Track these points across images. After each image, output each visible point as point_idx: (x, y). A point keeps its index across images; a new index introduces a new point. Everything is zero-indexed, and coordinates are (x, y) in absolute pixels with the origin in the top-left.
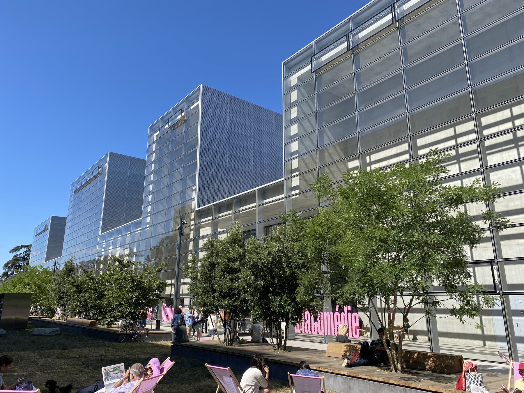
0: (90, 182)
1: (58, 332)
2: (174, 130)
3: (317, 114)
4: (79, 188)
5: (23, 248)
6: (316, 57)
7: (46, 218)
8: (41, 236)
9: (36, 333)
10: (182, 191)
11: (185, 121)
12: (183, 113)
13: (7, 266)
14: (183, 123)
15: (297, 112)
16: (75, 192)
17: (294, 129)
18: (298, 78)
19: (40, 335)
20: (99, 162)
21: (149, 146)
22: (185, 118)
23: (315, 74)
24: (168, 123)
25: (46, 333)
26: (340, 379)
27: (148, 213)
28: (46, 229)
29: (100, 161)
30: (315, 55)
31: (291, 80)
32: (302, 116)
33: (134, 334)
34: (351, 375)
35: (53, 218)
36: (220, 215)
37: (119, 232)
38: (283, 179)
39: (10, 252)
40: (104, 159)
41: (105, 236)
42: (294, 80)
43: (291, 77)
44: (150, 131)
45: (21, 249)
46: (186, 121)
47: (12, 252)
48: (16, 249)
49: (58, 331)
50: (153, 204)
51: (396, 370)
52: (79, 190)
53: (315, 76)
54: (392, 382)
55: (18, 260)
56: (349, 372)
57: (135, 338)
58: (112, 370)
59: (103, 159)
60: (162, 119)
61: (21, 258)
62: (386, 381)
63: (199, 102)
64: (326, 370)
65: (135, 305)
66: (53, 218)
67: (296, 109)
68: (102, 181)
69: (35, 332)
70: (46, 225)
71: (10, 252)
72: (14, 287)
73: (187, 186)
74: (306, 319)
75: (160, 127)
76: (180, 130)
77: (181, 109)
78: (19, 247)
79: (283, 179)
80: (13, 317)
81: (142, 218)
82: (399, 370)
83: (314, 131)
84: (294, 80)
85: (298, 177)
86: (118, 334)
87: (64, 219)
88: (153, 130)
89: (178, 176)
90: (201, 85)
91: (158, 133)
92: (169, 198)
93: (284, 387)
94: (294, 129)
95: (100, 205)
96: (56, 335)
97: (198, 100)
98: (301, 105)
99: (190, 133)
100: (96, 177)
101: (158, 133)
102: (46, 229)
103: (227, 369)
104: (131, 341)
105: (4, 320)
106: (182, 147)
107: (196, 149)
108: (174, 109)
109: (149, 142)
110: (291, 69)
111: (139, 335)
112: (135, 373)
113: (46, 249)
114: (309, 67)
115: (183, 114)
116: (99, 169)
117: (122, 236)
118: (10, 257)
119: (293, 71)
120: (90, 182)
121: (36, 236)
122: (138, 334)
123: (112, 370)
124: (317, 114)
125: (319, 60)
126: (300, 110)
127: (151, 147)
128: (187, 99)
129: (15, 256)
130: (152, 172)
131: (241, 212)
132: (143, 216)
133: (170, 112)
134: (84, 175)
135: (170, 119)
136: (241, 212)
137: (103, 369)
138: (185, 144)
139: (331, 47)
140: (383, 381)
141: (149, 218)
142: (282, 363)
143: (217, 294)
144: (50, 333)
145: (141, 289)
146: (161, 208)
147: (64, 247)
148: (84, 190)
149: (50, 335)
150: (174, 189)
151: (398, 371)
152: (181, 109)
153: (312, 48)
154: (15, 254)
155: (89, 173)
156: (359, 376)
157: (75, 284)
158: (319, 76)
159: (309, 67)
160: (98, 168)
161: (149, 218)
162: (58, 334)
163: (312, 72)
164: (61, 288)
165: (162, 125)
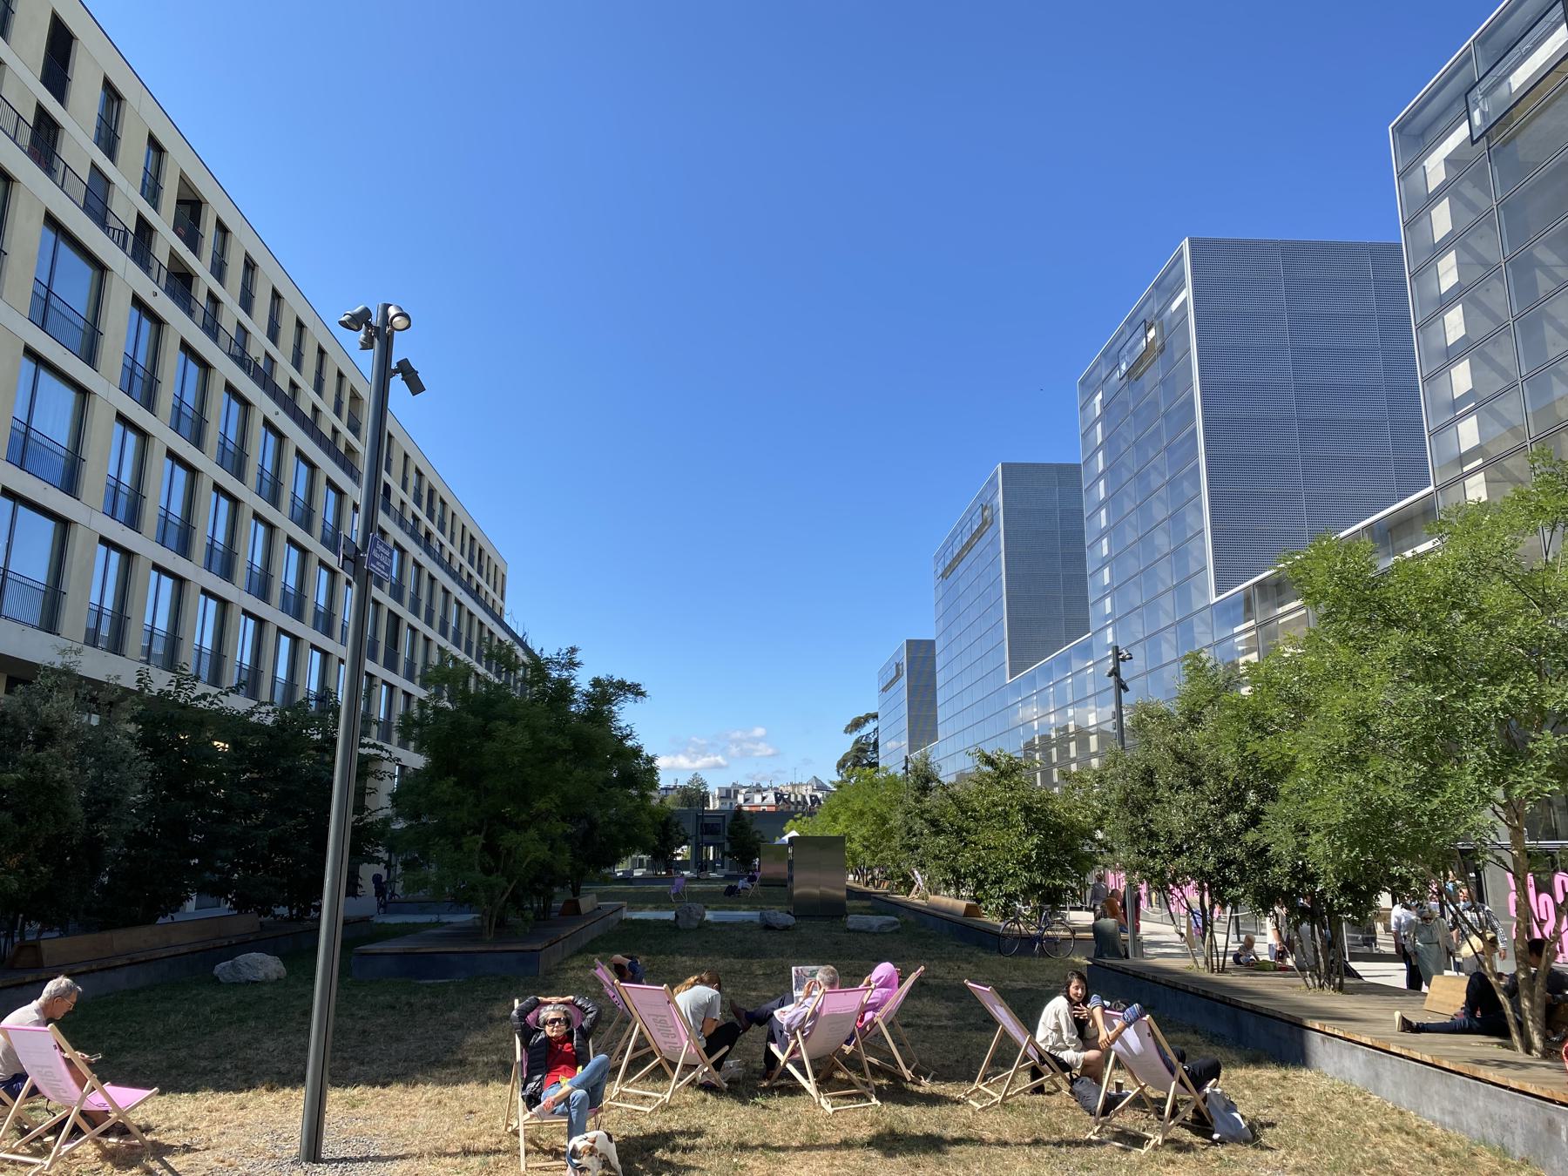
0: (968, 547)
1: (896, 927)
2: (1137, 379)
3: (1509, 271)
4: (950, 565)
5: (871, 721)
6: (1483, 86)
7: (892, 649)
8: (892, 690)
9: (851, 926)
10: (1174, 552)
11: (1161, 349)
12: (1149, 330)
13: (844, 766)
14: (1154, 360)
15: (1455, 270)
16: (942, 575)
17: (1454, 324)
18: (1448, 161)
19: (860, 931)
20: (982, 493)
21: (1084, 436)
22: (1158, 344)
23: (1488, 143)
24: (1118, 365)
25: (870, 928)
26: (1360, 1053)
27: (1107, 617)
28: (898, 676)
29: (985, 489)
30: (1480, 80)
31: (1428, 171)
32: (1480, 271)
33: (1039, 938)
34: (1377, 1045)
35: (908, 642)
36: (1280, 611)
37: (1047, 672)
38: (1431, 488)
39: (846, 732)
40: (992, 483)
41: (1034, 677)
42: (1435, 167)
43: (1426, 163)
44: (1082, 394)
45: (867, 724)
46: (1162, 351)
47: (851, 732)
48: (857, 724)
49: (895, 923)
50: (1114, 590)
51: (1528, 1048)
52: (950, 569)
53: (1489, 149)
54: (1446, 1064)
55: (866, 751)
56: (1376, 1039)
57: (1041, 948)
58: (808, 974)
59: (990, 482)
60: (1104, 354)
61: (869, 744)
62: (1436, 1064)
63: (1186, 294)
64: (1336, 1032)
65: (1041, 867)
66: (908, 642)
67: (1451, 258)
68: (994, 542)
69: (851, 923)
70: (897, 665)
71: (846, 732)
72: (835, 819)
73: (1190, 534)
74: (1544, 917)
75: (1104, 377)
76: (1153, 376)
77: (1145, 321)
78: (861, 718)
79: (1431, 488)
80: (816, 891)
81: (1093, 634)
82: (1536, 1049)
83: (1503, 327)
84: (1435, 167)
85: (1481, 476)
86: (997, 935)
87: (931, 644)
88: (1089, 387)
89: (1160, 512)
90: (1187, 240)
91: (1099, 396)
92: (1148, 571)
93: (1251, 1066)
94: (1454, 324)
95: (996, 605)
96: (891, 932)
97: (1182, 286)
98: (1470, 241)
99: (1174, 381)
100: (979, 534)
101: (1099, 396)
102: (898, 676)
103: (988, 990)
104: (1034, 955)
105: (801, 896)
106: (1158, 428)
107: (1190, 429)
108: (1129, 322)
109: (1084, 422)
110: (1419, 137)
111: (1051, 939)
112: (823, 980)
113: (905, 724)
114: (1462, 132)
115: (1152, 334)
116: (983, 510)
117: (1094, 664)
118: (847, 744)
119: (1428, 140)
120: (968, 547)
121: (883, 690)
122: (1048, 938)
123: (808, 974)
124: (1509, 271)
125: (1503, 91)
126: (1467, 258)
127: (1090, 436)
128: (1156, 286)
129: (857, 742)
130: (1101, 505)
131: (1284, 620)
132: (1093, 629)
133: (1121, 333)
134: (955, 530)
135: (1122, 354)
136: (1284, 620)
137: (793, 968)
138: (1166, 416)
139: (1524, 45)
140: (1430, 1061)
141: (1110, 631)
142: (1264, 1012)
143: (1162, 846)
144: (881, 926)
145: (1049, 826)
146: (1136, 599)
147: (942, 715)
148: (961, 568)
149: (880, 932)
150: (1549, 332)
151: (1534, 1052)
152: (1145, 321)
153: (1470, 63)
154: (856, 735)
155: (964, 524)
156: (1392, 1050)
157: (926, 816)
158: (1505, 144)
159: (1462, 132)
160: (980, 510)
161: (1110, 631)
162: (897, 932)
163: (1474, 143)
164: (911, 824)
165: (1107, 373)
